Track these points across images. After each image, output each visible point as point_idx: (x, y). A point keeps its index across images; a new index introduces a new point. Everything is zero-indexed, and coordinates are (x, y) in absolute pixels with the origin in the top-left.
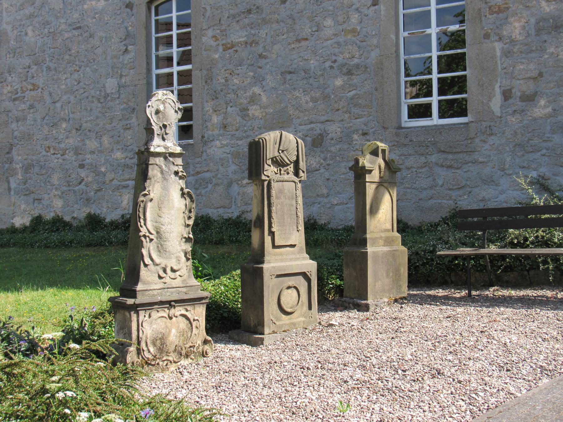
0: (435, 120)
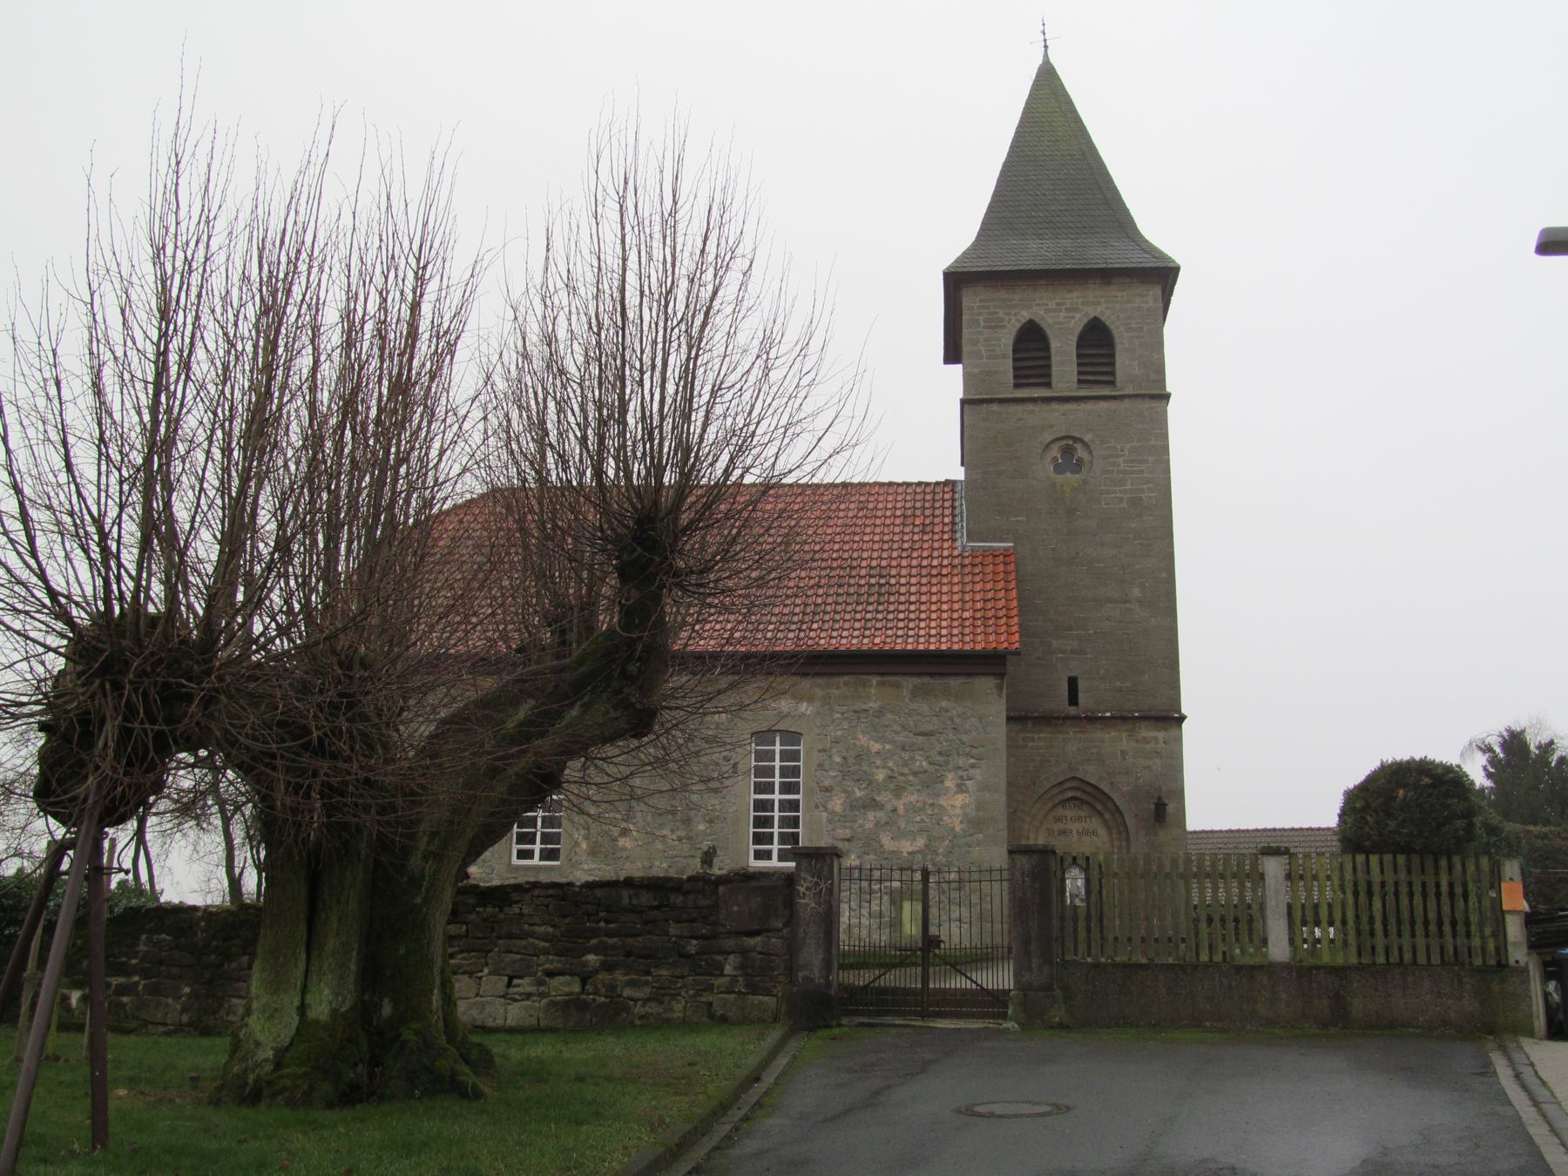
0: (536, 861)
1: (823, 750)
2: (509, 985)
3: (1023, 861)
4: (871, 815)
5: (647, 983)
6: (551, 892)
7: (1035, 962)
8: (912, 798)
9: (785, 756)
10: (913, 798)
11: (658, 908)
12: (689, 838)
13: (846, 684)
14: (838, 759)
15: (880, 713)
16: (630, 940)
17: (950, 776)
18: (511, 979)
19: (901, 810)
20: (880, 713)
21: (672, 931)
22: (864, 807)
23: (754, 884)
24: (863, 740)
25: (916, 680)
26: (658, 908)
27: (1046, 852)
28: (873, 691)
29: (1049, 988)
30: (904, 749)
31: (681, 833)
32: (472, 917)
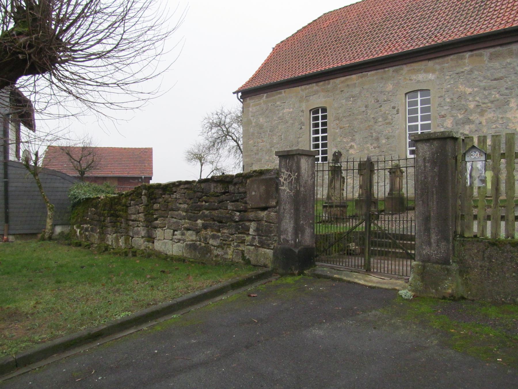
1: (441, 97)
2: (173, 235)
3: (425, 149)
4: (467, 127)
5: (218, 237)
6: (186, 186)
7: (434, 238)
8: (490, 115)
9: (423, 102)
10: (491, 115)
11: (224, 193)
12: (379, 147)
13: (451, 60)
14: (448, 100)
15: (471, 71)
16: (213, 212)
17: (513, 100)
18: (174, 231)
19: (484, 123)
20: (471, 71)
21: (230, 207)
22: (463, 123)
23: (263, 177)
24: (461, 88)
25: (492, 50)
26: (224, 193)
27: (447, 139)
28: (467, 61)
29: (446, 262)
30: (485, 89)
31: (376, 145)
32: (160, 200)
